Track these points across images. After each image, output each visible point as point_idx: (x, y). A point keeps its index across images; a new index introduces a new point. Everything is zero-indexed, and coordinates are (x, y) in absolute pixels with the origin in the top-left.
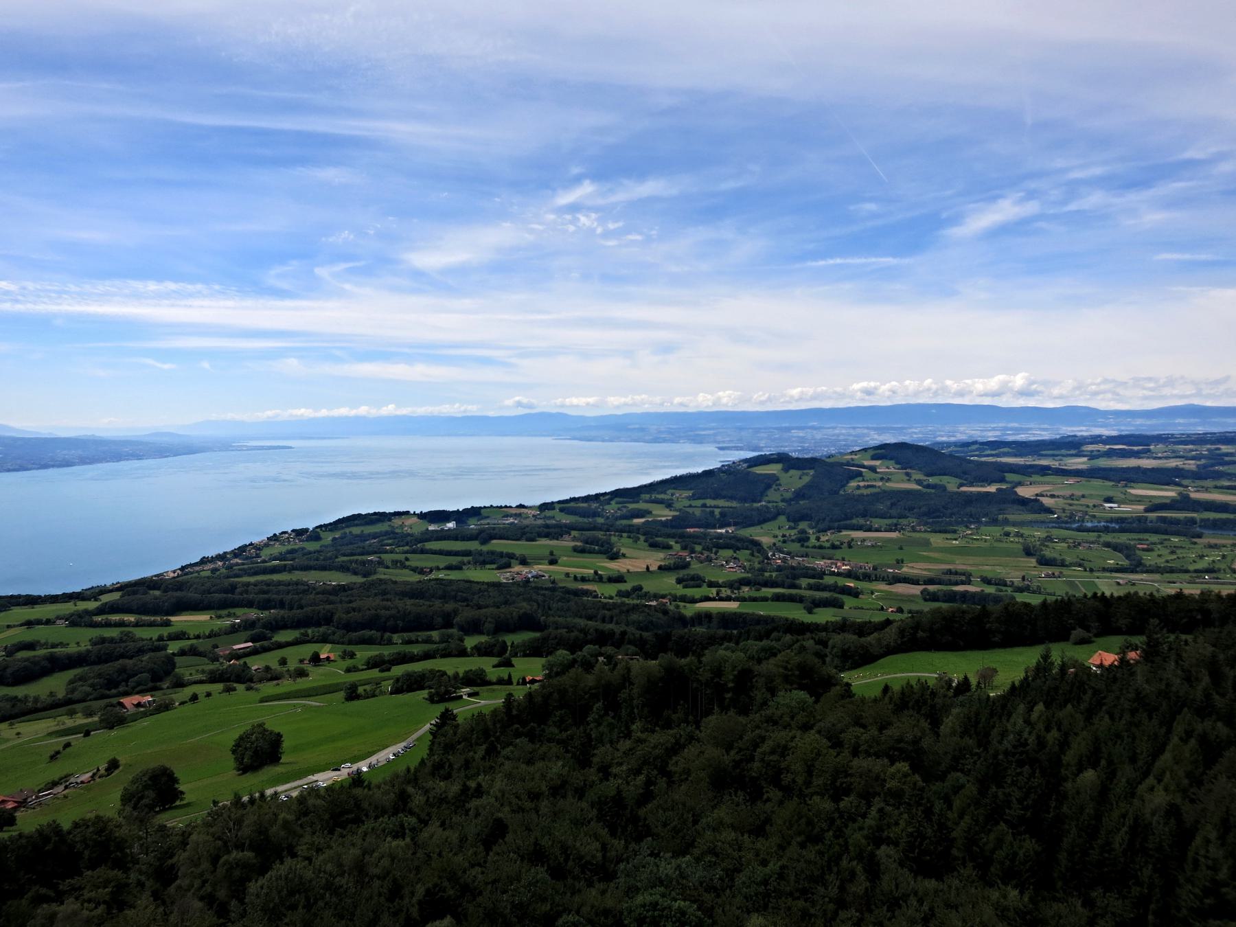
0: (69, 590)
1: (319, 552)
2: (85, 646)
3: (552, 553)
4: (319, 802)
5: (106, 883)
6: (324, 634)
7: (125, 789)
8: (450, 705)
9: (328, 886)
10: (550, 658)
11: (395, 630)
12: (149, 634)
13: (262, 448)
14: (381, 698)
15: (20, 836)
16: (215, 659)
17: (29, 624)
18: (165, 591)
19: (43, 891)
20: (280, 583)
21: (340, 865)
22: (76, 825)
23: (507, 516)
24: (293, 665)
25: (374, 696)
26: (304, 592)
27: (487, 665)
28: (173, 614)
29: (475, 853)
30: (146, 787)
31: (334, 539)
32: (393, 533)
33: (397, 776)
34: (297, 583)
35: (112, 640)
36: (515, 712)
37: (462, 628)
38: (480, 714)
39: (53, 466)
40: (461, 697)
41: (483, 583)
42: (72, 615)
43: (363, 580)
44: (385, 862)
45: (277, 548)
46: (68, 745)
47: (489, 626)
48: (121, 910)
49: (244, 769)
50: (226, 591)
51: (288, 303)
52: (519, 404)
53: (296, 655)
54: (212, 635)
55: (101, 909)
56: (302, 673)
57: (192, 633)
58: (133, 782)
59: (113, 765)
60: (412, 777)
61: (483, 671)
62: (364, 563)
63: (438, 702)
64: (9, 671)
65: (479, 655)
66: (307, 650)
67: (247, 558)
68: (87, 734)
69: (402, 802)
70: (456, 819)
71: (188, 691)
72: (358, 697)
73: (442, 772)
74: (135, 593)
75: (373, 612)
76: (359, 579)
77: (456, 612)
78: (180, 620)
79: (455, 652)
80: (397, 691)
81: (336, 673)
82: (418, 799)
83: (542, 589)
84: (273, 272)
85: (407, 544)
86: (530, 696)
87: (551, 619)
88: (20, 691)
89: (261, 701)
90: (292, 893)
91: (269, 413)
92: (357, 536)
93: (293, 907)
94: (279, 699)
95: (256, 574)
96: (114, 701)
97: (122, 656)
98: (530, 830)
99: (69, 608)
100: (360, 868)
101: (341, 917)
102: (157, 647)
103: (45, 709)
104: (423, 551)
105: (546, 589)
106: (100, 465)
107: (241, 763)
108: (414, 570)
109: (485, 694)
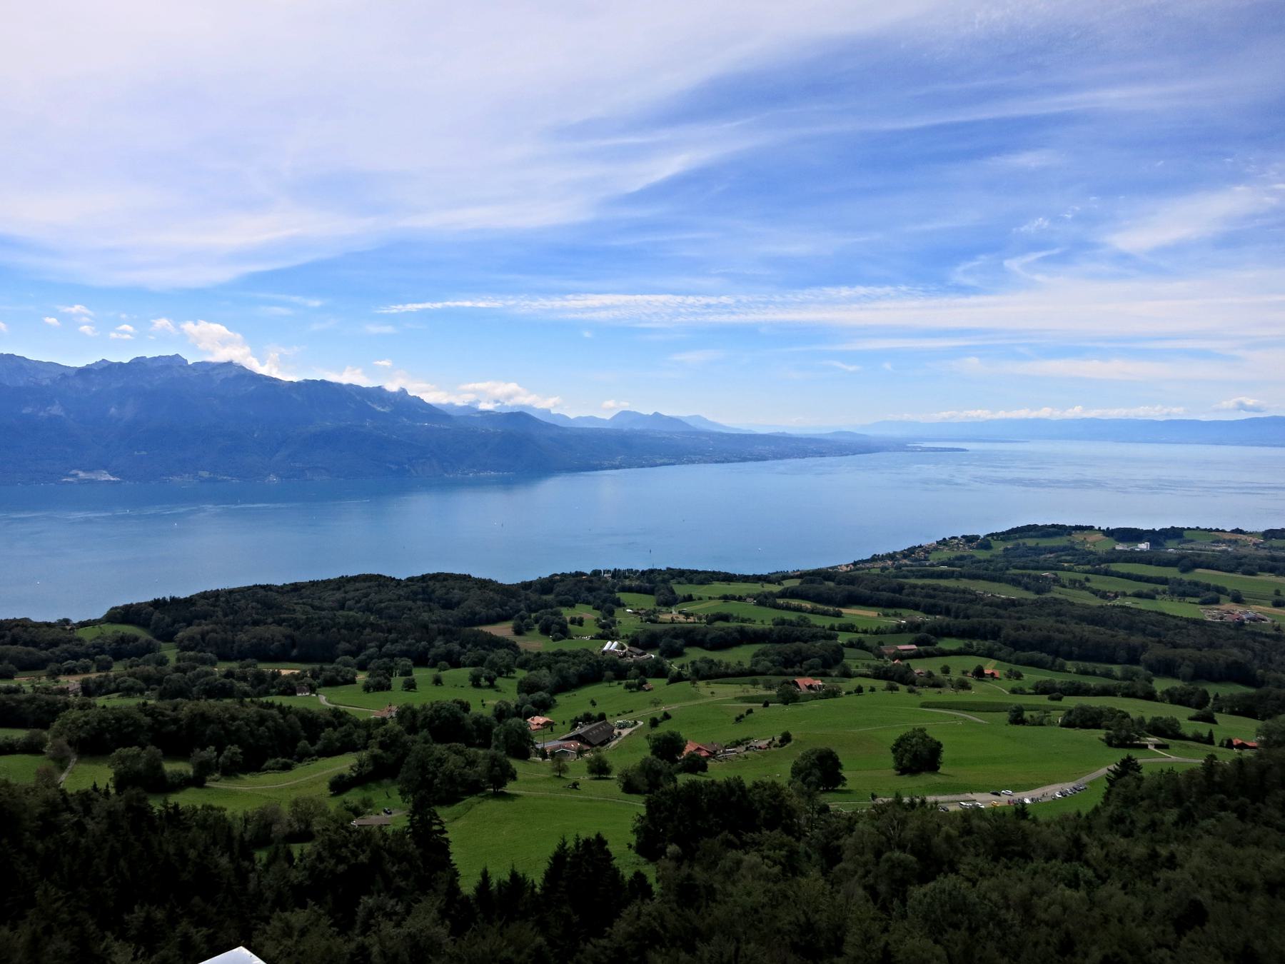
0: (759, 573)
1: (989, 561)
2: (768, 625)
3: (1277, 593)
4: (984, 824)
5: (781, 846)
6: (989, 649)
7: (796, 763)
8: (1134, 753)
9: (992, 916)
10: (1268, 722)
11: (1069, 657)
12: (825, 622)
13: (936, 450)
14: (1048, 728)
15: (713, 782)
16: (880, 656)
17: (726, 598)
18: (839, 583)
19: (731, 837)
20: (947, 589)
21: (1006, 898)
22: (756, 785)
23: (1218, 542)
24: (955, 675)
25: (1041, 724)
26: (971, 601)
27: (1182, 715)
28: (844, 606)
29: (1163, 932)
30: (813, 765)
31: (1006, 549)
32: (1073, 549)
33: (1067, 819)
34: (964, 592)
35: (791, 623)
36: (1217, 778)
37: (1150, 667)
38: (1171, 772)
39: (750, 460)
40: (1146, 747)
41: (1181, 619)
42: (759, 595)
43: (1036, 597)
44: (1056, 910)
45: (946, 554)
46: (750, 711)
47: (1186, 669)
48: (794, 874)
49: (903, 770)
50: (894, 591)
51: (973, 300)
52: (1242, 407)
53: (961, 666)
54: (878, 632)
55: (777, 869)
56: (964, 686)
57: (860, 627)
58: (803, 758)
59: (786, 738)
60: (1087, 823)
61: (1176, 721)
62: (1037, 578)
63: (1117, 746)
64: (709, 637)
65: (1172, 702)
66: (972, 662)
67: (916, 560)
68: (766, 705)
69: (1076, 851)
70: (1140, 885)
71: (854, 683)
72: (1023, 722)
73: (1121, 827)
74: (812, 582)
75: (1045, 633)
76: (1031, 596)
77: (1144, 647)
78: (852, 614)
79: (1140, 693)
80: (1068, 724)
81: (999, 691)
82: (1094, 852)
83: (1261, 635)
84: (960, 269)
85: (1089, 563)
86: (1240, 763)
87: (1272, 674)
88: (716, 656)
89: (923, 706)
90: (954, 911)
91: (945, 414)
92: (1030, 548)
93: (956, 926)
94: (944, 708)
95: (923, 577)
96: (790, 679)
97: (798, 639)
98: (1238, 926)
99: (757, 588)
100: (1026, 908)
101: (1003, 953)
102: (829, 635)
103: (726, 675)
104: (1107, 573)
105: (1267, 636)
106: (788, 461)
107: (900, 764)
108: (1095, 592)
109: (1176, 749)
